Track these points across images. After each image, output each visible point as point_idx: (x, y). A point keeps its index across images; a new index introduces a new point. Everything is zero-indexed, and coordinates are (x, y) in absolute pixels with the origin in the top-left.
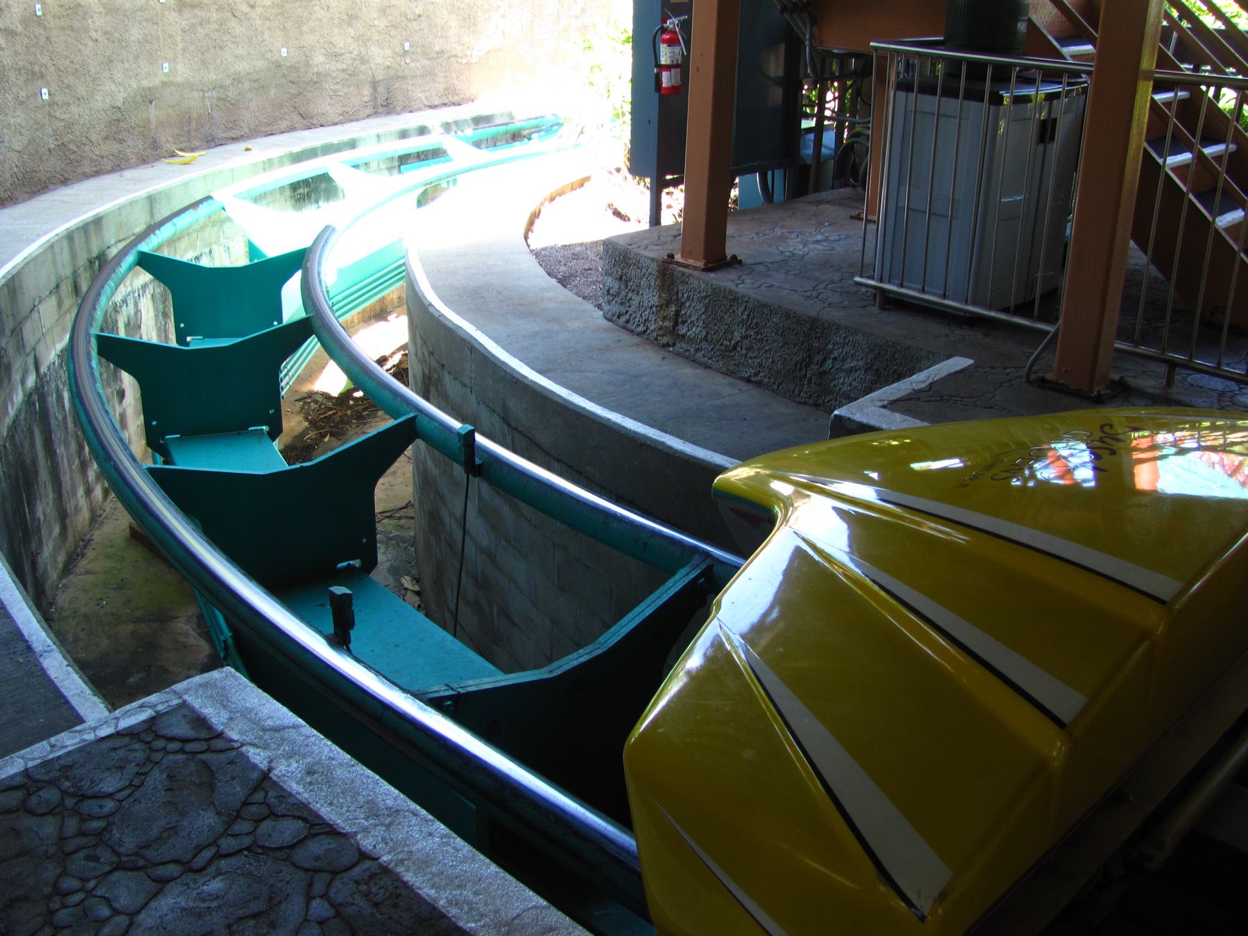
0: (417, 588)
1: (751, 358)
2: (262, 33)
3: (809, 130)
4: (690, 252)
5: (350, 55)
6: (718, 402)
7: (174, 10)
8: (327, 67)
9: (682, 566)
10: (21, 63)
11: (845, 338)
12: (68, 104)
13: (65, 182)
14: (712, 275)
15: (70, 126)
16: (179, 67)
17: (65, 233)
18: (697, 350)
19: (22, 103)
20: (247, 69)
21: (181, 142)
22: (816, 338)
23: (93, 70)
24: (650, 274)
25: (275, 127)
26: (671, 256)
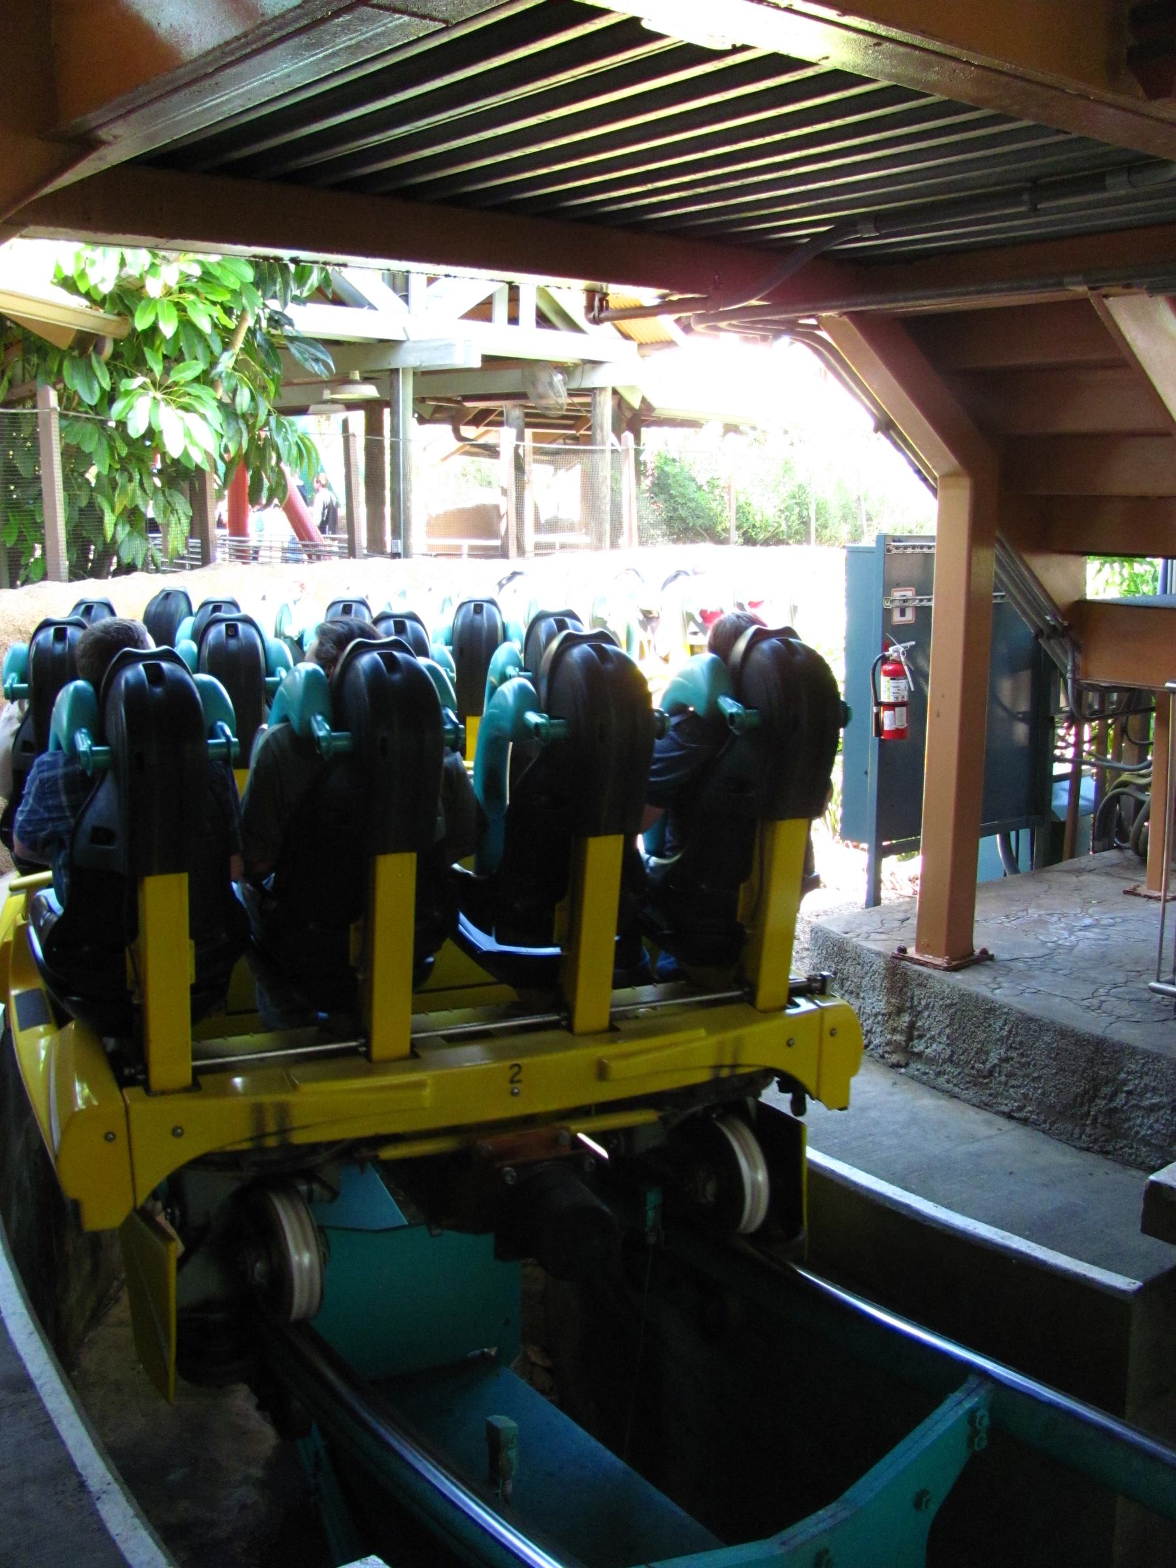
0: (548, 1363)
1: (1013, 1087)
3: (1062, 778)
4: (928, 945)
6: (973, 1147)
9: (953, 1389)
11: (1144, 1065)
14: (958, 976)
18: (939, 1074)
24: (875, 972)
26: (903, 950)
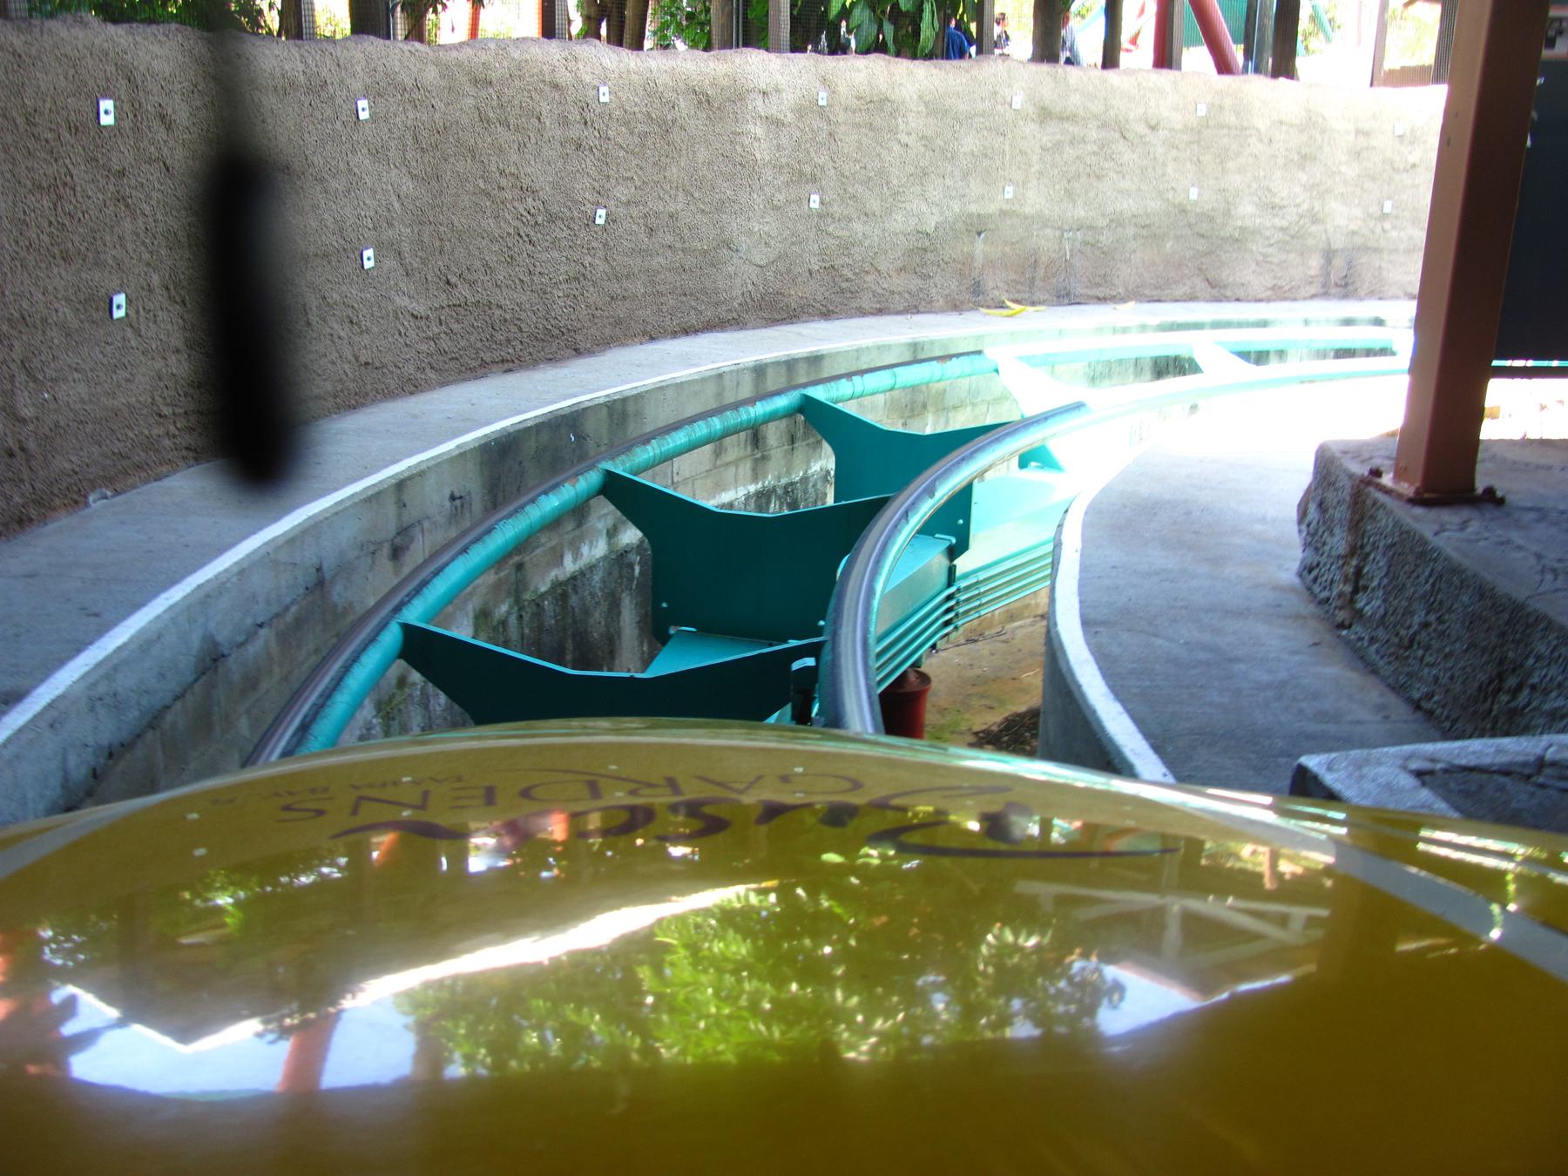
2: (1164, 164)
5: (1295, 210)
7: (1033, 120)
8: (1258, 221)
10: (784, 161)
12: (850, 220)
13: (827, 315)
15: (846, 247)
16: (1030, 194)
17: (751, 364)
19: (776, 208)
20: (1133, 209)
21: (1018, 292)
22: (1513, 641)
23: (895, 182)
25: (1166, 292)
